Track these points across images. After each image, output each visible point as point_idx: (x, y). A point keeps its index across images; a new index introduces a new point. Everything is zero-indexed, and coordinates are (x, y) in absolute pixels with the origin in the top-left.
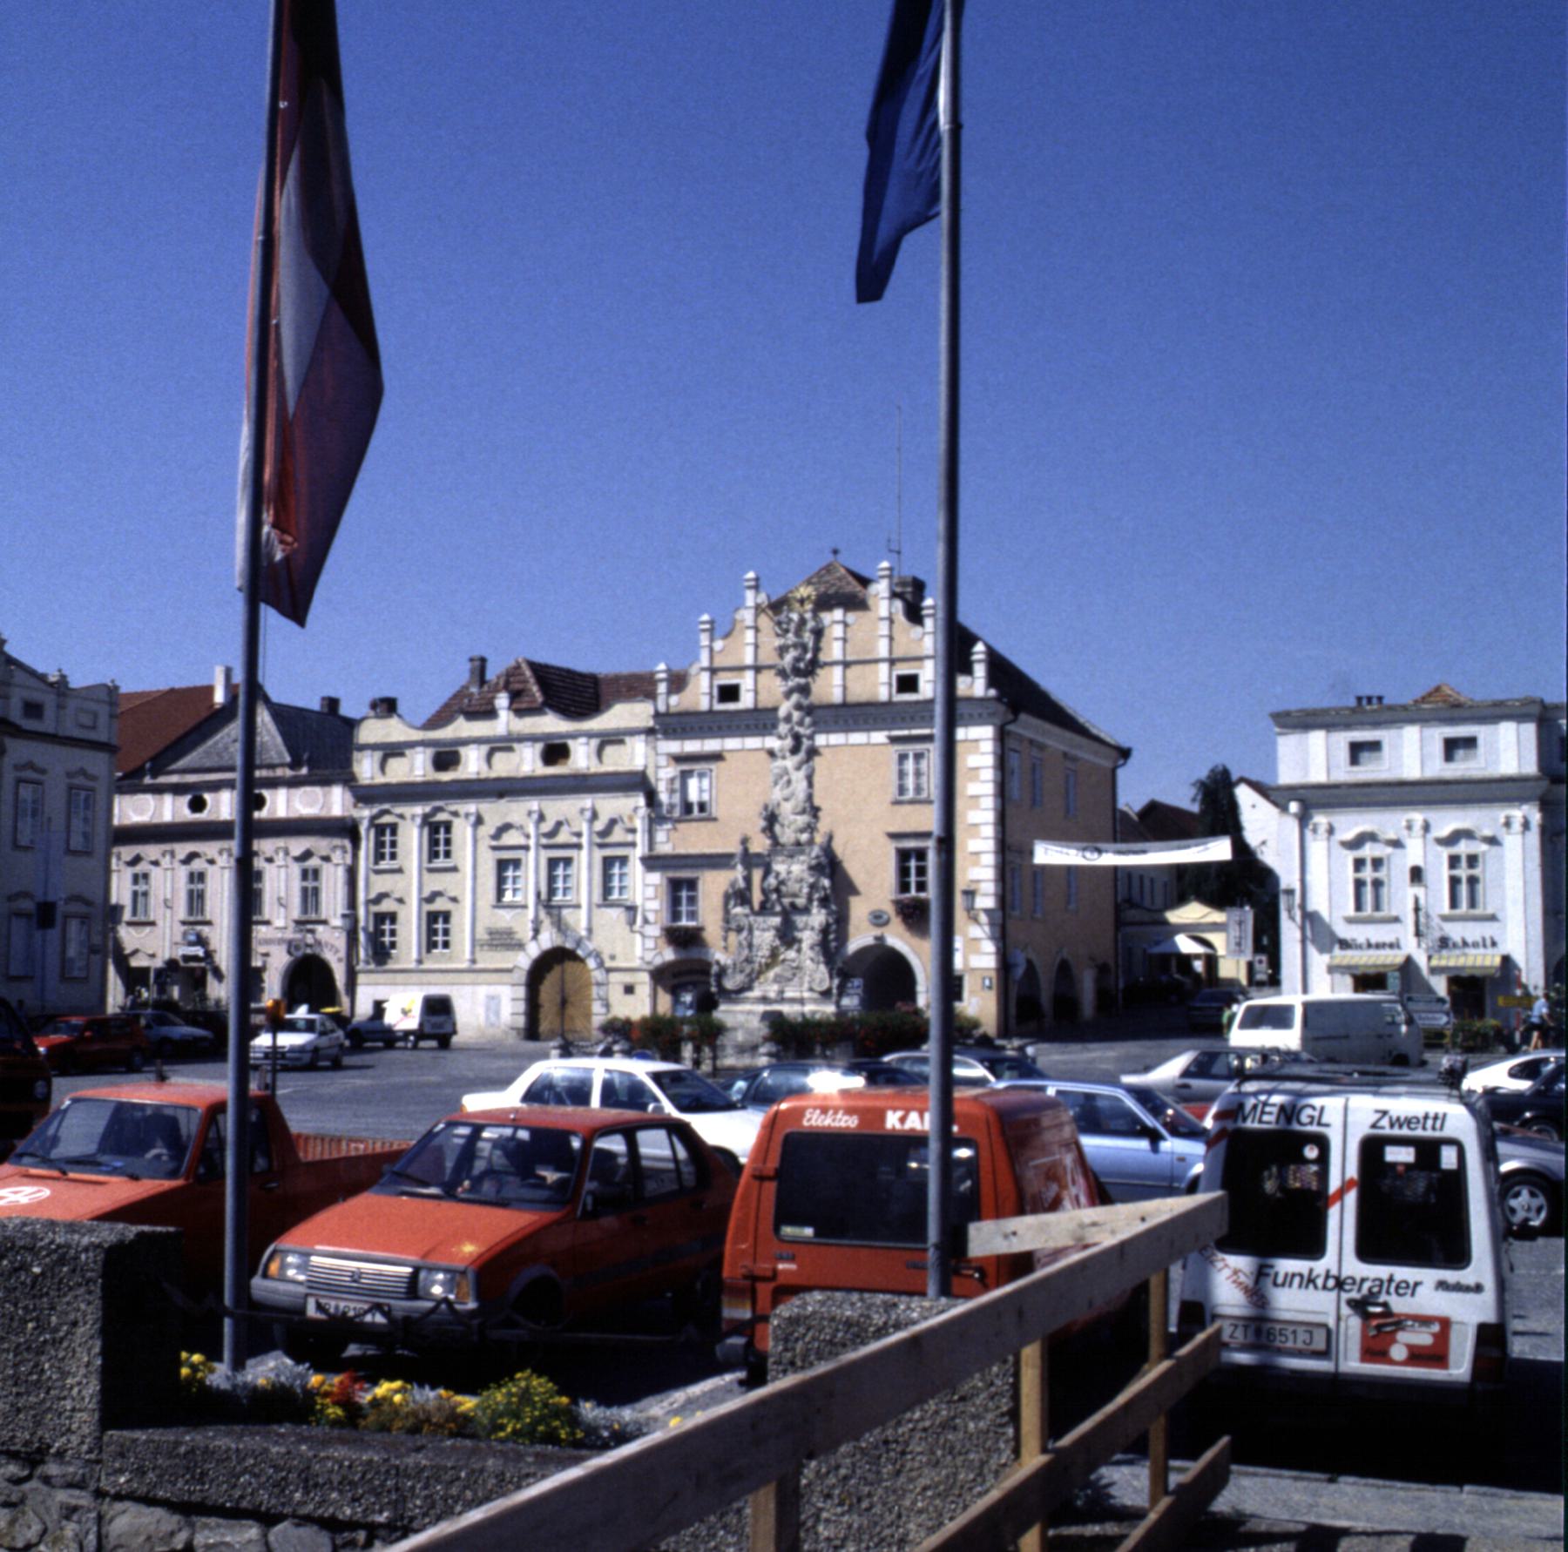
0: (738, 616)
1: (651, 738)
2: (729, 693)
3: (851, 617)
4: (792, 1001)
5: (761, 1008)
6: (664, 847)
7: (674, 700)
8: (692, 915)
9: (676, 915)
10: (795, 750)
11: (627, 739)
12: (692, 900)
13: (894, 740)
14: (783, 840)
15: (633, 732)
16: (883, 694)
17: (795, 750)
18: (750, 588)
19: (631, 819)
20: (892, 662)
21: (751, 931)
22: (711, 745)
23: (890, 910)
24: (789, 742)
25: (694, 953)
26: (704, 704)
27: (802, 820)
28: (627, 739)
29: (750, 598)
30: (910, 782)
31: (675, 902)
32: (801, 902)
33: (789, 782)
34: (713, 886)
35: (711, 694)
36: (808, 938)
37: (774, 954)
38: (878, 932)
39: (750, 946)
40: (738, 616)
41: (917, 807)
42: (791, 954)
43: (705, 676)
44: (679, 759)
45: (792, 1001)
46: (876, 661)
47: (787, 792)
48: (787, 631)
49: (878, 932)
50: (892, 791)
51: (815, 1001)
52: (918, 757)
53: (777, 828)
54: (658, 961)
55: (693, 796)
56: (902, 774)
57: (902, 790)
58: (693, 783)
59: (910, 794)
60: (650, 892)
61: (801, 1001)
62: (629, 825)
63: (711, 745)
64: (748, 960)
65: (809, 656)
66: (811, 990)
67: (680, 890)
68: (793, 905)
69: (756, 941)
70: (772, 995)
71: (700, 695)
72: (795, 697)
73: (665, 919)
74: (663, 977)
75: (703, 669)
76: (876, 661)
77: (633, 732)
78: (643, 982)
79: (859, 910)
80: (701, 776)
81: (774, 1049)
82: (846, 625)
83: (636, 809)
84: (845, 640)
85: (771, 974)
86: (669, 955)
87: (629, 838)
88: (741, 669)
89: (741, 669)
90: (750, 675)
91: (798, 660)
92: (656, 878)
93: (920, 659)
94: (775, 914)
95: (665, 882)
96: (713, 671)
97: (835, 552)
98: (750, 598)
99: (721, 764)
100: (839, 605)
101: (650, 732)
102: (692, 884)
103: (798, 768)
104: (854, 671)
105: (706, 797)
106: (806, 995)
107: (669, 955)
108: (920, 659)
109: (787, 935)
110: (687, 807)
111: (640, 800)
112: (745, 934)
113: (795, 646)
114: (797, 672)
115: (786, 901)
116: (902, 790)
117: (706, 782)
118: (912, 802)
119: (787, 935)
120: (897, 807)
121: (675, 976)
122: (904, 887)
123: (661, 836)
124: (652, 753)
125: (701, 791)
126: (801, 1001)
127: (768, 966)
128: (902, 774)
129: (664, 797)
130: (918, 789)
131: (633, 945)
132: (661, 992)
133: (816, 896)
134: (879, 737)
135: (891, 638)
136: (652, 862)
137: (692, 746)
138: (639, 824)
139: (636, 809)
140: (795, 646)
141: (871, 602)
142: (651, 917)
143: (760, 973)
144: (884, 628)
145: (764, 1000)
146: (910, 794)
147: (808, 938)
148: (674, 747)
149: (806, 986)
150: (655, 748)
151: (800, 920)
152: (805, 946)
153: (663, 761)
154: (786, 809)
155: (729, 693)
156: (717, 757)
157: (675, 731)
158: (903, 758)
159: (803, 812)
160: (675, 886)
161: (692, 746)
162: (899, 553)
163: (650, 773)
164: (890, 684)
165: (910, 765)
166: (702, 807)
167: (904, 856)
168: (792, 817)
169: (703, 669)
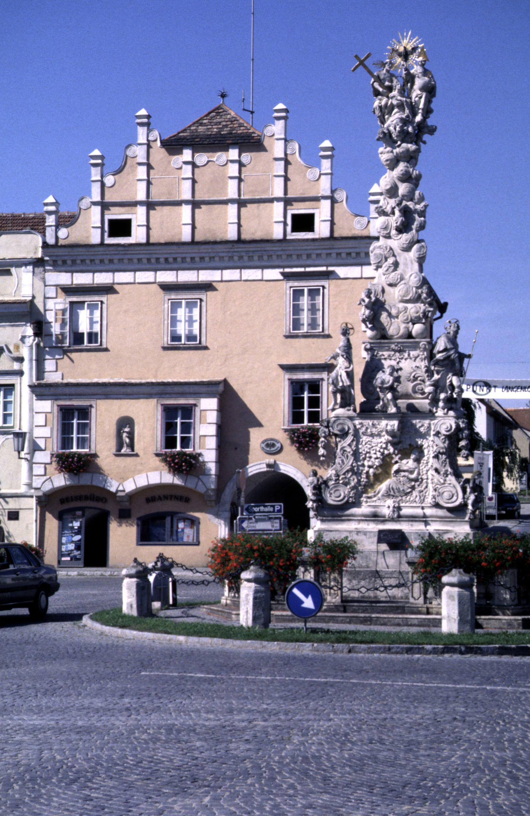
0: (130, 152)
1: (39, 270)
2: (121, 228)
3: (246, 157)
4: (412, 518)
5: (374, 527)
6: (52, 377)
7: (63, 233)
8: (82, 442)
9: (66, 442)
10: (403, 229)
11: (13, 270)
12: (84, 428)
13: (287, 277)
14: (391, 331)
15: (21, 263)
16: (277, 233)
17: (403, 229)
18: (142, 124)
19: (17, 347)
20: (288, 202)
21: (357, 436)
22: (102, 278)
23: (283, 438)
24: (396, 219)
25: (85, 479)
26: (95, 238)
27: (415, 309)
28: (13, 270)
29: (142, 134)
30: (305, 317)
31: (66, 429)
32: (423, 403)
33: (396, 265)
34: (105, 415)
35: (102, 228)
36: (431, 445)
37: (386, 463)
38: (271, 460)
39: (356, 454)
40: (130, 152)
41: (310, 340)
42: (409, 463)
43: (97, 210)
44: (68, 290)
45: (412, 518)
46: (271, 201)
47: (393, 276)
48: (390, 89)
49: (271, 460)
50: (287, 325)
51: (442, 519)
52: (313, 293)
53: (384, 317)
54: (48, 487)
55: (84, 327)
56: (297, 310)
57: (297, 324)
58: (84, 315)
59: (305, 329)
60: (40, 420)
61: (425, 520)
62: (15, 354)
63: (102, 278)
64: (355, 471)
65: (419, 118)
66: (437, 505)
67: (72, 420)
68: (411, 408)
69: (363, 448)
70: (386, 512)
71: (90, 229)
72: (402, 167)
73: (55, 446)
74: (50, 503)
75: (94, 203)
76: (271, 201)
77: (21, 263)
78: (29, 509)
79: (256, 437)
80: (92, 307)
81: (261, 574)
82: (241, 165)
83: (23, 338)
84: (240, 180)
85: (383, 487)
86: (60, 480)
87: (16, 366)
88: (134, 204)
89: (134, 204)
90: (141, 210)
91: (405, 122)
92: (46, 405)
93: (316, 199)
94: (390, 417)
95: (56, 408)
96: (105, 206)
97: (223, 96)
98: (142, 134)
99: (112, 297)
100: (234, 145)
101: (38, 263)
102: (84, 413)
103: (407, 249)
104: (248, 211)
105: (97, 328)
106: (429, 512)
107: (60, 480)
108: (316, 199)
109: (406, 442)
110: (78, 338)
111: (29, 330)
112: (350, 438)
113: (401, 106)
114: (405, 136)
115: (402, 403)
116: (297, 324)
117: (97, 314)
118: (306, 336)
119: (406, 442)
120: (289, 340)
121: (62, 501)
122: (297, 417)
123: (49, 365)
124: (39, 284)
125: (92, 322)
126: (425, 520)
127: (378, 478)
128: (297, 310)
129: (56, 329)
130: (313, 324)
131: (18, 471)
132: (49, 516)
133: (442, 396)
134: (274, 274)
135: (286, 179)
136: (41, 390)
137: (82, 279)
138: (25, 352)
139: (23, 338)
140: (401, 106)
141: (266, 143)
142: (41, 443)
143: (369, 486)
144: (279, 168)
145: (375, 517)
146: (305, 329)
147: (431, 445)
148: (64, 278)
149: (429, 500)
150: (44, 280)
151: (421, 424)
152: (429, 452)
153: (51, 292)
154: (393, 297)
155: (121, 228)
156: (108, 289)
157: (64, 262)
158: (297, 294)
159: (417, 299)
160: (66, 414)
161: (82, 279)
162: (252, 112)
163: (39, 303)
164: (285, 224)
165: (305, 301)
166: (93, 337)
167: (297, 387)
168: (401, 305)
169: (94, 203)
